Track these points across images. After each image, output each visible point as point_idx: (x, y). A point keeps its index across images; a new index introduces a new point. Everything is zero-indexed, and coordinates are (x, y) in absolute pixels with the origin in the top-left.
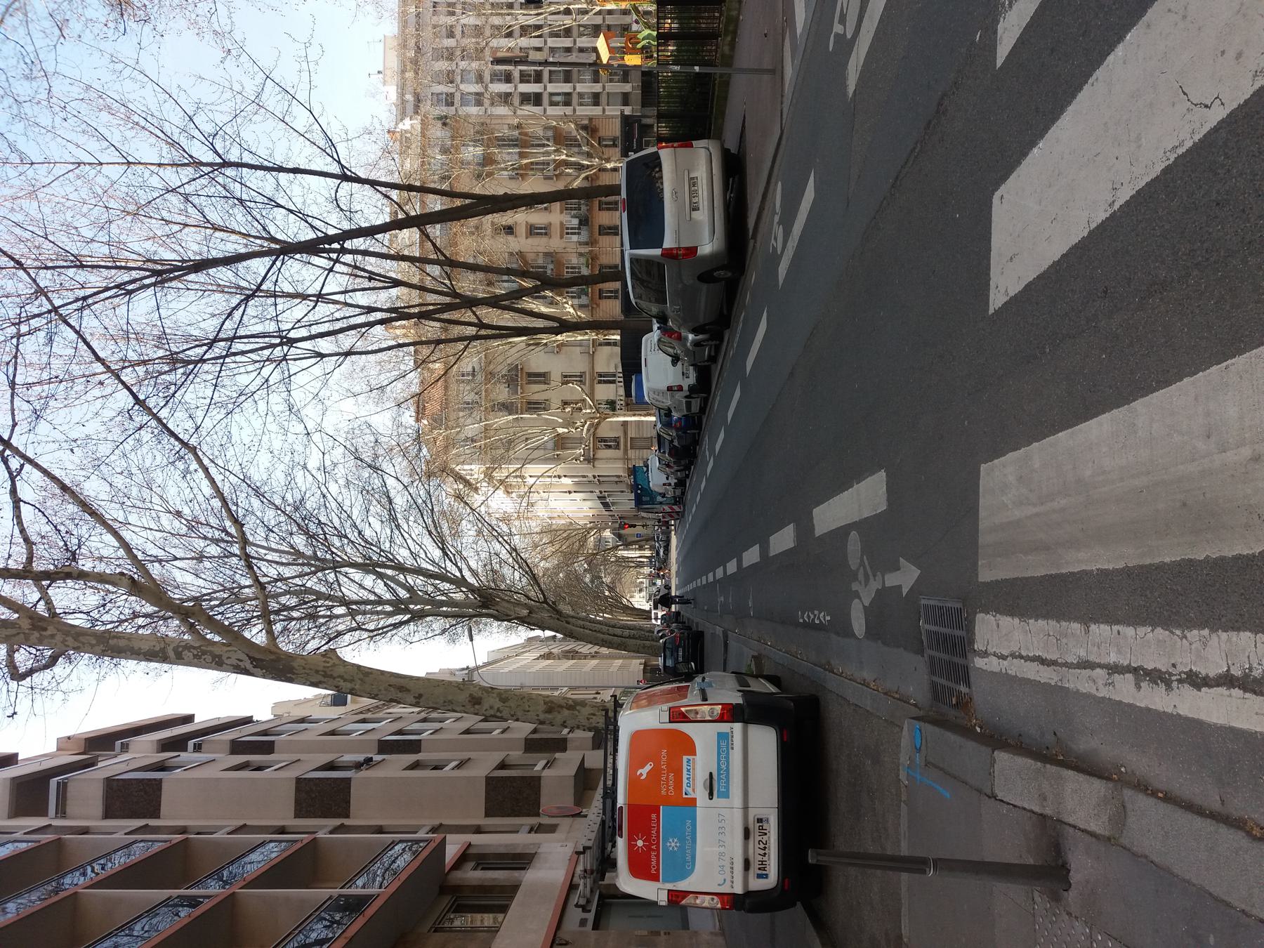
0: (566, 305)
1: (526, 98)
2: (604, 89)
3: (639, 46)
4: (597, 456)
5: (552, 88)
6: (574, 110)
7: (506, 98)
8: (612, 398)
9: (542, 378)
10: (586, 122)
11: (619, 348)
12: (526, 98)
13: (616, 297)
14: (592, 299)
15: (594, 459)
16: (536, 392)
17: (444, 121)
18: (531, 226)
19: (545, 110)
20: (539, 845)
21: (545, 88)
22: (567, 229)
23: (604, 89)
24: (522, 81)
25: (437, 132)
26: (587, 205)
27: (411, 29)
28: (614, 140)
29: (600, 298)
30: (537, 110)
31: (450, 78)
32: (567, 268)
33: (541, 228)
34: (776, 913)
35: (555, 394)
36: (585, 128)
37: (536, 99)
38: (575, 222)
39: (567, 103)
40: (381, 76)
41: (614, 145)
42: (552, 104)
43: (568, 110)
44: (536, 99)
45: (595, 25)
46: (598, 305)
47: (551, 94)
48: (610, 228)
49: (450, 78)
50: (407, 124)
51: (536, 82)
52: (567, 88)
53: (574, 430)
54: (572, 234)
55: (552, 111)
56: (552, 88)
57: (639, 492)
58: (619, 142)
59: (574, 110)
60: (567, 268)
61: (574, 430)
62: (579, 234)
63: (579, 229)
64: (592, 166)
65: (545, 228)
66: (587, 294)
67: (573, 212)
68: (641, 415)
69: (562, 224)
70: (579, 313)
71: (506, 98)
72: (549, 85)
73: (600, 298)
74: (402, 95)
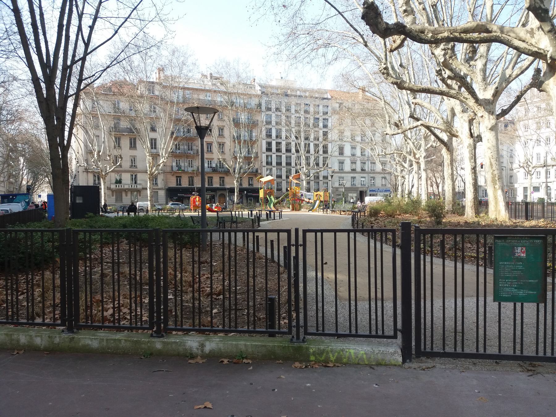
0: (164, 158)
1: (269, 144)
2: (283, 180)
3: (268, 197)
4: (89, 174)
5: (274, 156)
6: (264, 167)
7: (269, 136)
8: (123, 182)
9: (133, 145)
10: (259, 172)
11: (92, 185)
12: (269, 144)
13: (177, 184)
14: (176, 173)
15: (87, 172)
16: (125, 142)
17: (260, 105)
18: (212, 144)
19: (265, 153)
20: (344, 145)
21: (284, 154)
22: (211, 162)
23: (283, 180)
24: (276, 143)
25: (254, 102)
26: (222, 171)
27: (298, 93)
28: (252, 185)
29: (176, 176)
30: (264, 149)
31: (277, 109)
32: (192, 161)
33: (210, 149)
34: (307, 276)
35: (126, 151)
36: (257, 171)
37: (269, 149)
38: (214, 165)
39: (268, 163)
40: (280, 78)
41: (249, 185)
42: (267, 156)
43: (264, 164)
44: (269, 149)
45: (282, 176)
46: (173, 175)
47: (271, 156)
48: (211, 182)
49: (277, 109)
50: (258, 88)
51: (267, 148)
52: (274, 163)
53: (93, 160)
54: (208, 164)
55: (264, 156)
56: (274, 156)
57: (11, 197)
58: (251, 187)
59: (264, 167)
60: (192, 161)
61: (93, 160)
62: (208, 167)
63: (211, 167)
64: (235, 174)
65: (211, 151)
66: (178, 170)
67: (218, 165)
68: (105, 197)
69: (213, 159)
70: (161, 165)
71: (269, 136)
72: (275, 155)
73: (176, 176)
74: (272, 87)
